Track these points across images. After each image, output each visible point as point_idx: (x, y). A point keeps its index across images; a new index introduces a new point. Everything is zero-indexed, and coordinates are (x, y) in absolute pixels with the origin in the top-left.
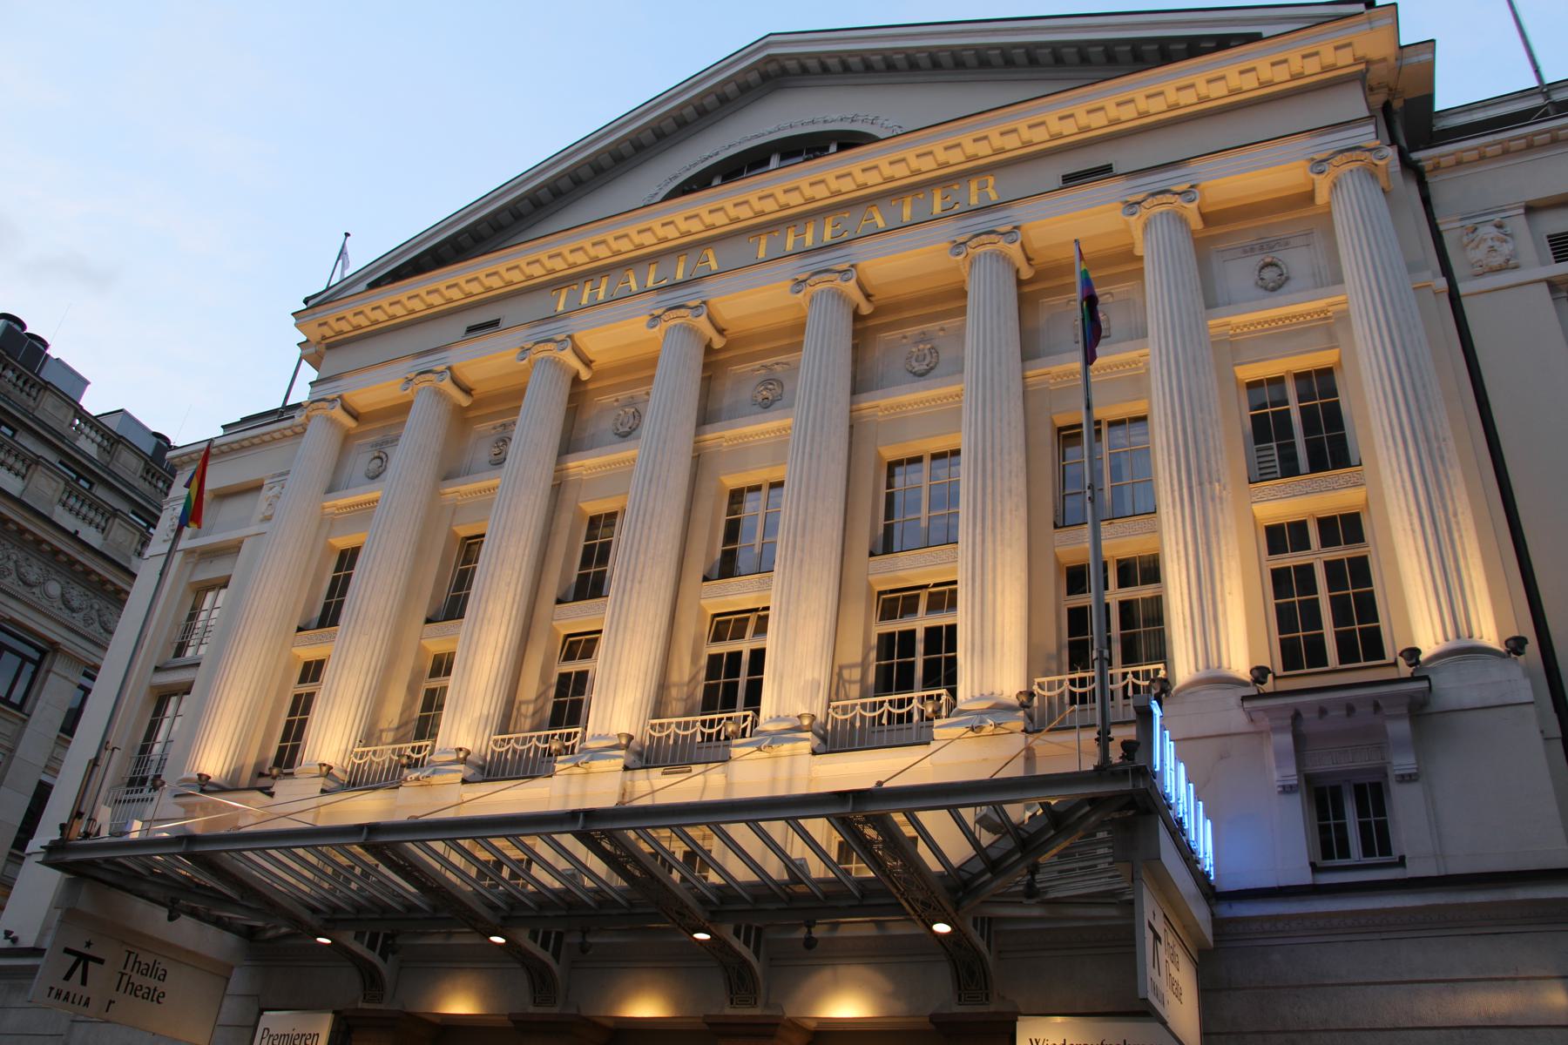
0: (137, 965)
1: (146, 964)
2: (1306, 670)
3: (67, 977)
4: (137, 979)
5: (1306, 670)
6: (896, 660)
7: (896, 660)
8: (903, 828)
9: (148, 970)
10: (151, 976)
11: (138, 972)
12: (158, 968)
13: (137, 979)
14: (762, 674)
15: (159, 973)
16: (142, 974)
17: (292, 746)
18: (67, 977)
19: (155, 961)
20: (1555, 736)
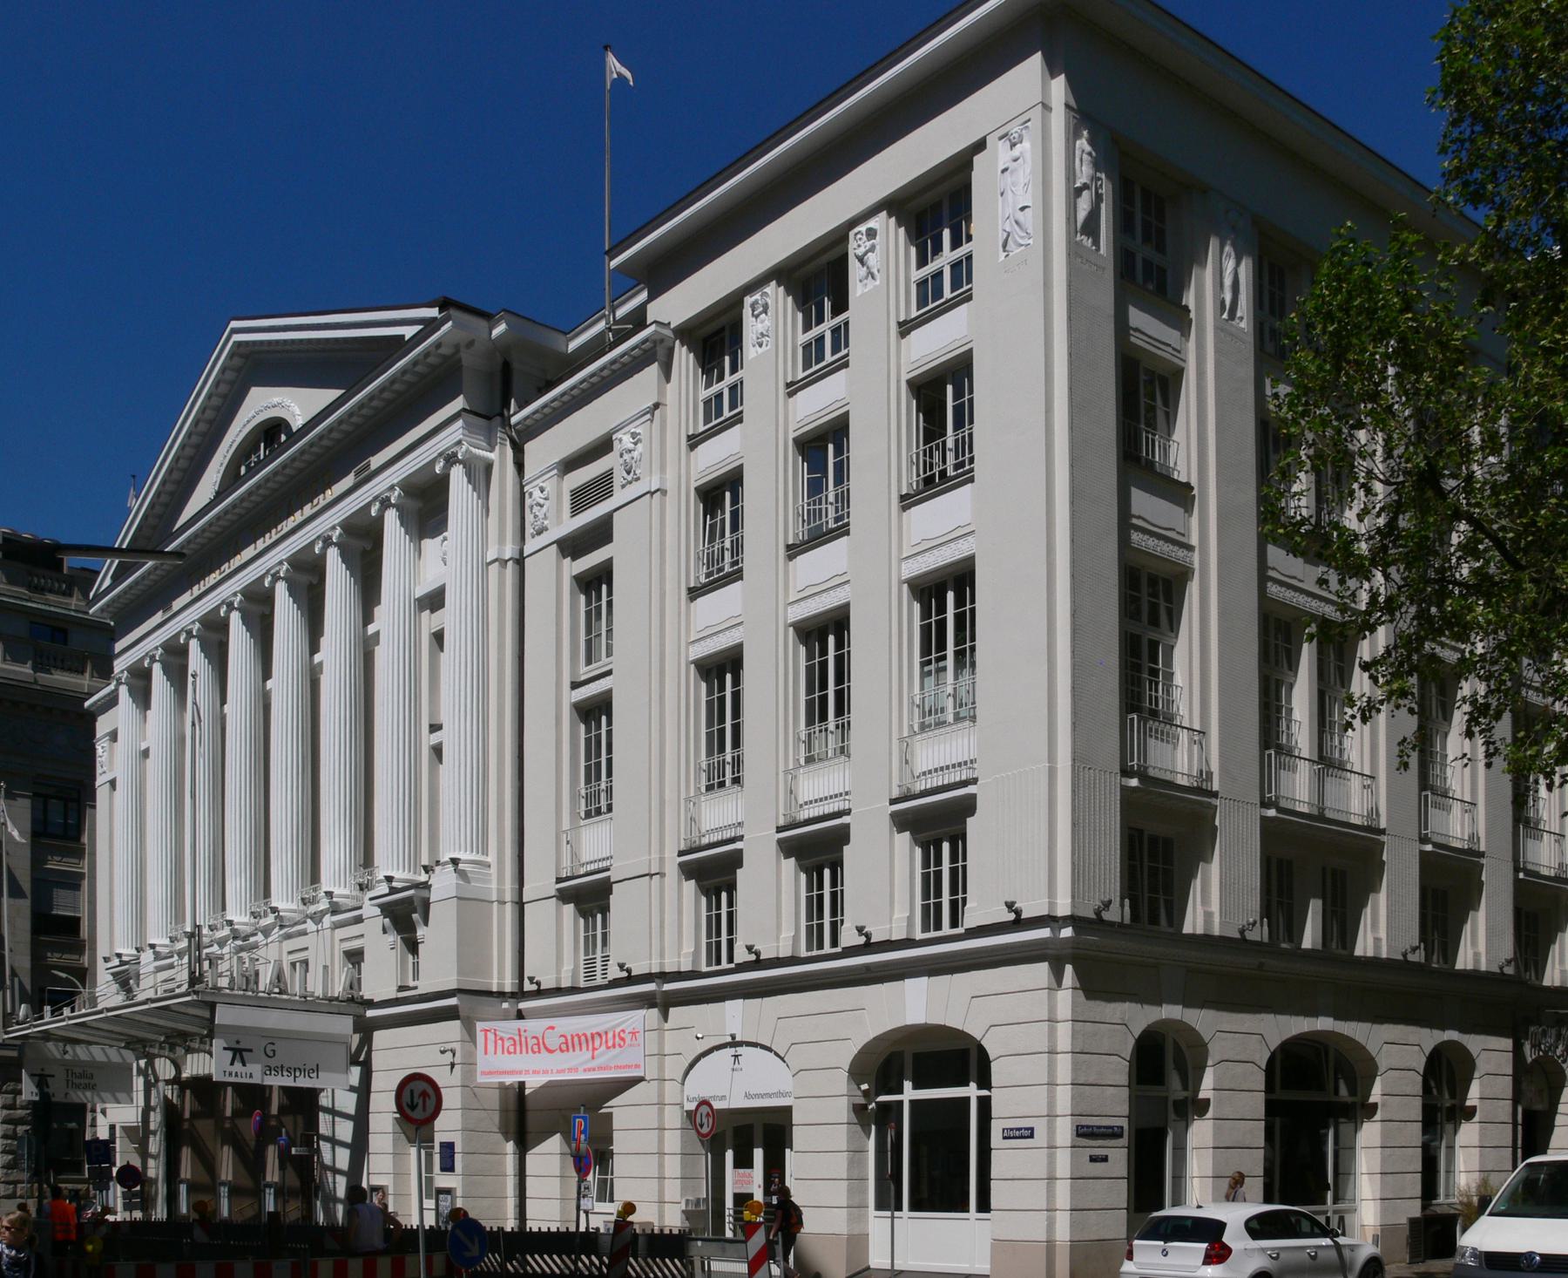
0: (500, 1042)
1: (534, 1037)
2: (806, 476)
3: (232, 1064)
4: (77, 1081)
5: (806, 476)
6: (932, 901)
7: (932, 901)
8: (189, 592)
9: (515, 1045)
10: (521, 1052)
11: (503, 1053)
12: (526, 1038)
13: (77, 1081)
14: (922, 874)
15: (530, 1046)
16: (509, 1053)
17: (819, 697)
18: (232, 1064)
19: (519, 1030)
20: (1045, 1161)
